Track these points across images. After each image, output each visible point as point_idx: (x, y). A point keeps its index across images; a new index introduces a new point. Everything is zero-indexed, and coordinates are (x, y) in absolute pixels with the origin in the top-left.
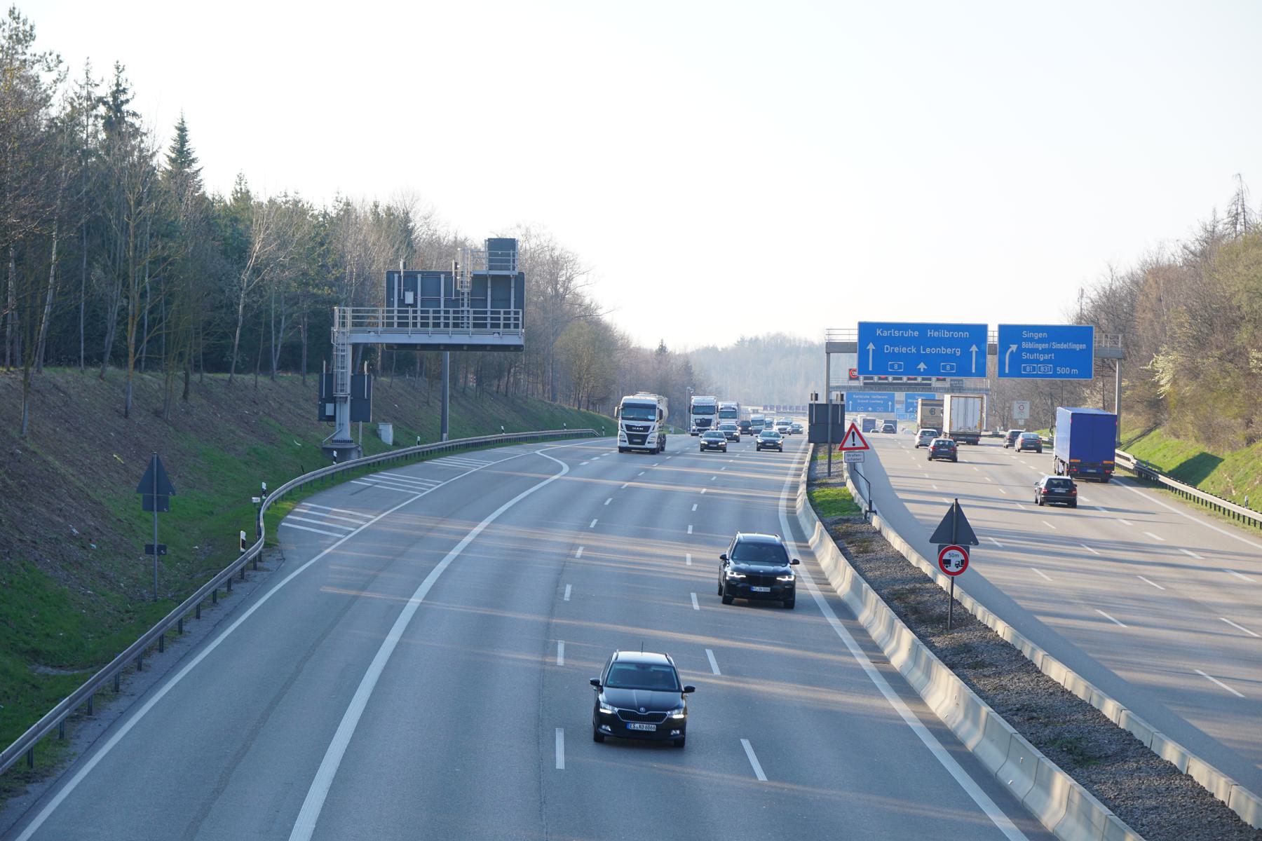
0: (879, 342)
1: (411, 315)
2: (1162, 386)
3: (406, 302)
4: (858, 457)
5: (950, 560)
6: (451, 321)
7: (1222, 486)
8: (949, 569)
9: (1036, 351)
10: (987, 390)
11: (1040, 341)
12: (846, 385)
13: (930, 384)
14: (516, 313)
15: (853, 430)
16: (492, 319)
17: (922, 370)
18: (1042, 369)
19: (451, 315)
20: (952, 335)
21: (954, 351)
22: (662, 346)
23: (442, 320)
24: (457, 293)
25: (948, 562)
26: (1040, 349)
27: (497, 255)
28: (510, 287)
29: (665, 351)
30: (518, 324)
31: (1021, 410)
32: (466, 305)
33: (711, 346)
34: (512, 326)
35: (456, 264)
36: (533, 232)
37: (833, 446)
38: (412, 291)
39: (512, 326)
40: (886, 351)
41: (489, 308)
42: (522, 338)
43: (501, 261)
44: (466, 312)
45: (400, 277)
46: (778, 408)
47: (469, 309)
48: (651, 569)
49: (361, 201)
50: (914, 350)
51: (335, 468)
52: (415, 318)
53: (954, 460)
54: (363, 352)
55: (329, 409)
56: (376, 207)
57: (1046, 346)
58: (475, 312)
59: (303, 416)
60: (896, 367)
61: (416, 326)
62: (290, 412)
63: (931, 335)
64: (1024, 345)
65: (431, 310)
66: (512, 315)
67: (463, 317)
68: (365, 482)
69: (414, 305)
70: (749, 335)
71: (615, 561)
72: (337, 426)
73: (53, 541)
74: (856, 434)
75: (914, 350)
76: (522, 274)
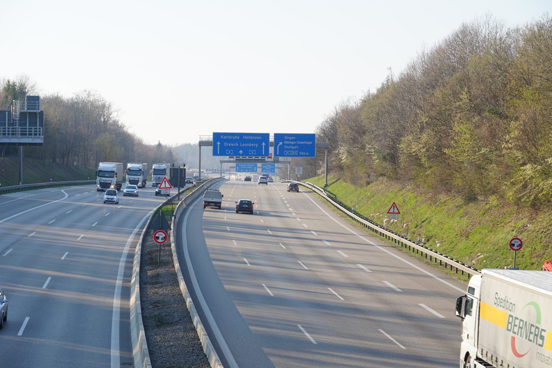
0: (222, 141)
2: (343, 160)
5: (159, 237)
7: (354, 203)
9: (290, 145)
10: (290, 162)
11: (292, 140)
13: (265, 160)
14: (40, 129)
16: (29, 131)
17: (241, 153)
18: (293, 153)
20: (254, 138)
21: (255, 145)
22: (159, 143)
23: (7, 132)
24: (13, 120)
25: (514, 245)
26: (309, 144)
27: (31, 103)
28: (27, 118)
31: (299, 170)
32: (17, 125)
33: (188, 143)
34: (38, 135)
39: (38, 135)
40: (225, 145)
41: (28, 127)
42: (42, 140)
43: (33, 106)
44: (17, 129)
46: (212, 170)
47: (18, 127)
48: (57, 241)
49: (3, 79)
50: (237, 145)
56: (9, 82)
58: (21, 129)
60: (229, 152)
63: (245, 138)
64: (285, 142)
66: (38, 130)
71: (44, 238)
75: (237, 145)
76: (42, 112)
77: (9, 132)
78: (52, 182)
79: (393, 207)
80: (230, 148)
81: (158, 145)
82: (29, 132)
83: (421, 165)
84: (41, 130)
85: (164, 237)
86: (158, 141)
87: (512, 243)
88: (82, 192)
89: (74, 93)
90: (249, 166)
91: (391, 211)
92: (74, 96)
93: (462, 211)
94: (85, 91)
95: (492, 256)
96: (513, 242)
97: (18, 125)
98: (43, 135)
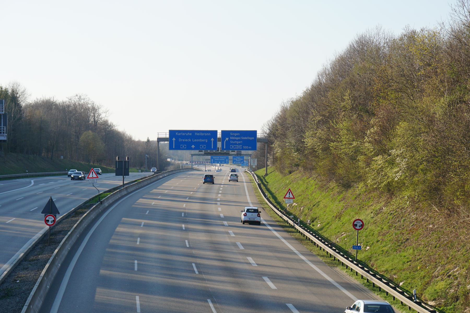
0: (177, 138)
5: (357, 224)
8: (48, 223)
9: (236, 140)
10: (251, 155)
11: (237, 136)
14: (4, 128)
17: (193, 148)
18: (238, 147)
20: (186, 134)
22: (148, 140)
25: (356, 225)
31: (254, 162)
34: (2, 133)
36: (82, 98)
37: (125, 177)
42: (6, 138)
46: (198, 162)
50: (190, 140)
53: (213, 183)
57: (239, 138)
60: (183, 146)
64: (231, 138)
75: (190, 140)
79: (288, 193)
80: (185, 143)
81: (146, 142)
83: (317, 157)
84: (5, 129)
85: (53, 220)
86: (147, 138)
87: (355, 223)
88: (46, 182)
89: (67, 98)
90: (222, 159)
91: (287, 196)
92: (67, 100)
93: (341, 196)
94: (77, 95)
95: (352, 235)
96: (355, 223)
98: (6, 133)
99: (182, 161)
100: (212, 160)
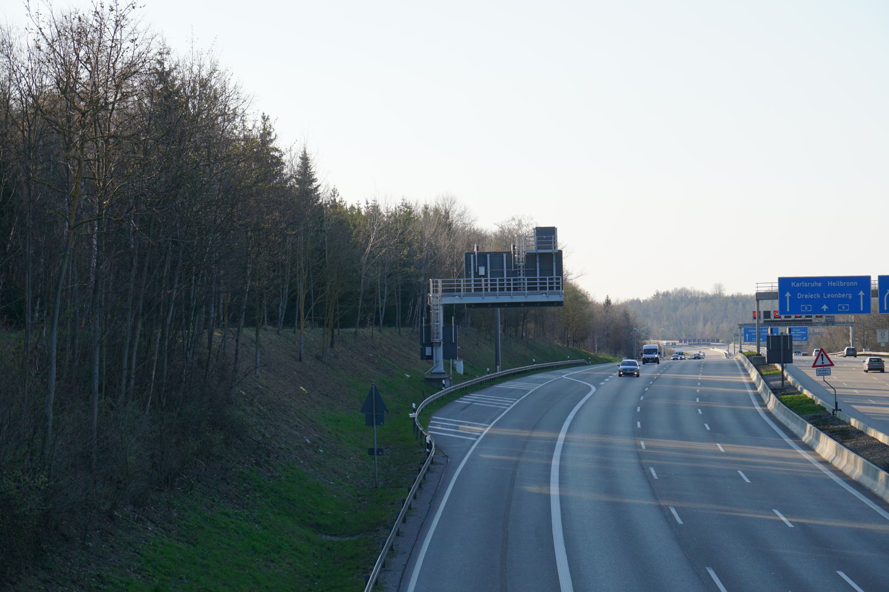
0: (794, 291)
1: (483, 283)
3: (480, 274)
4: (826, 372)
6: (512, 286)
10: (852, 323)
12: (751, 322)
15: (822, 353)
16: (541, 284)
17: (825, 310)
19: (512, 282)
20: (846, 284)
22: (608, 300)
23: (505, 286)
24: (515, 266)
27: (542, 239)
28: (553, 261)
29: (610, 304)
30: (560, 287)
32: (522, 275)
35: (514, 246)
36: (523, 222)
37: (785, 365)
38: (483, 266)
41: (538, 276)
44: (522, 280)
45: (474, 257)
51: (444, 392)
52: (486, 285)
53: (882, 371)
54: (449, 310)
55: (428, 351)
59: (405, 357)
60: (843, 307)
61: (487, 291)
62: (396, 354)
63: (830, 285)
65: (498, 279)
67: (520, 283)
68: (465, 400)
69: (486, 276)
70: (662, 290)
72: (435, 363)
73: (298, 448)
74: (824, 355)
77: (512, 289)
78: (535, 365)
82: (540, 285)
89: (496, 224)
94: (514, 219)
97: (523, 274)
99: (659, 340)
100: (747, 335)
